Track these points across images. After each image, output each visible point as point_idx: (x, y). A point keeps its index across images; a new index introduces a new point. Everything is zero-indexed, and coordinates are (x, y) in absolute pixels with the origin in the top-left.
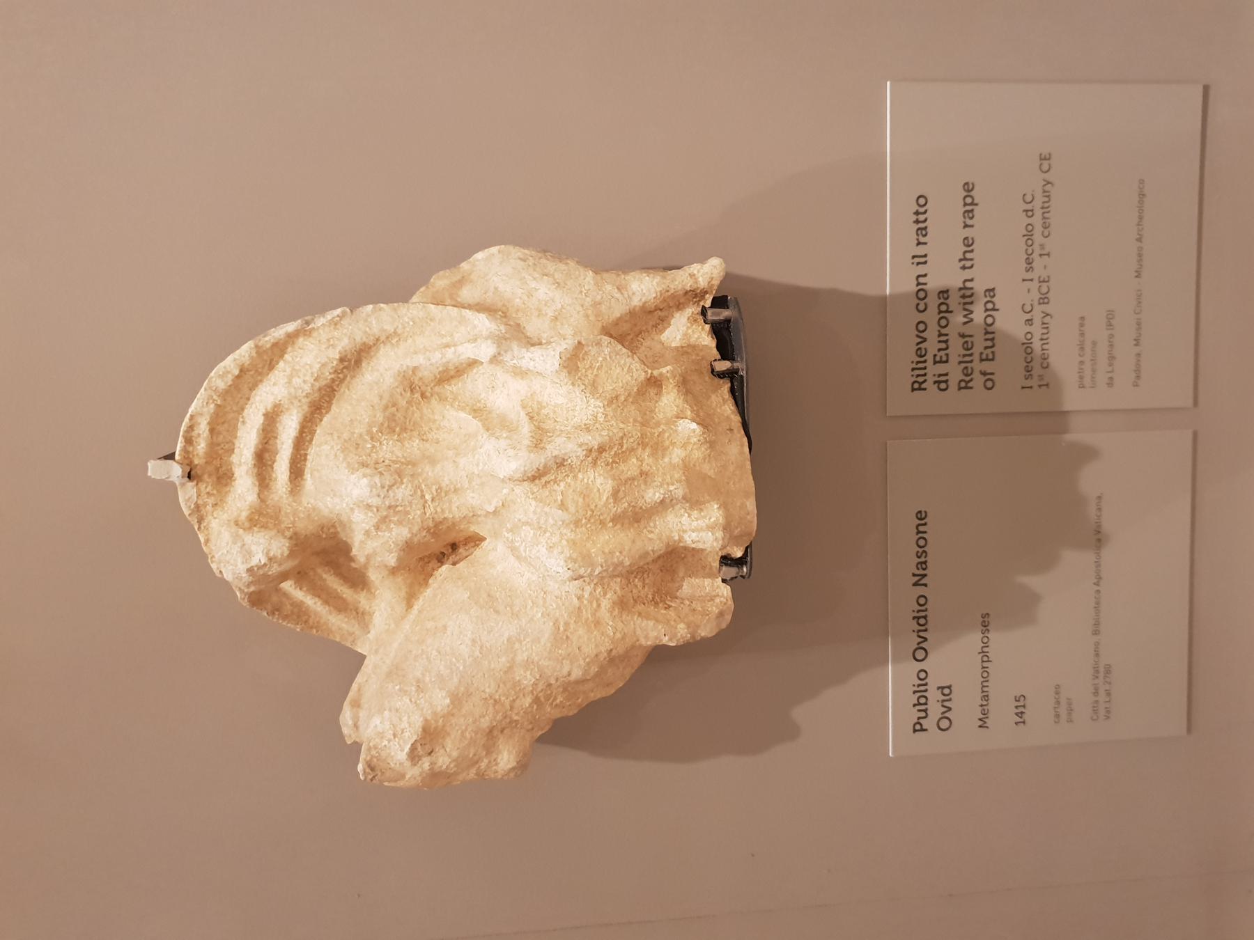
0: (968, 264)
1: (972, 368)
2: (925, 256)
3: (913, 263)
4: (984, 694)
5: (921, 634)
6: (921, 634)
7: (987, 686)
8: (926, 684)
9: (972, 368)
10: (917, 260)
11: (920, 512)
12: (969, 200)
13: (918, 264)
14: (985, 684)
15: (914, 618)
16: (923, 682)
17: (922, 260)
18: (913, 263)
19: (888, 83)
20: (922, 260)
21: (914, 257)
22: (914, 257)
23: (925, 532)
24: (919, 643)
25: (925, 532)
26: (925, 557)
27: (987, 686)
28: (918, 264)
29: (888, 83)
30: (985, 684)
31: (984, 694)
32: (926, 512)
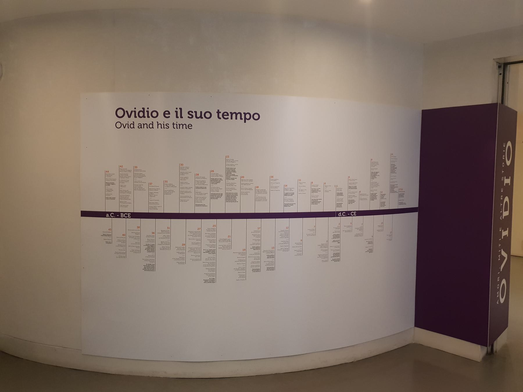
0: (175, 126)
1: (228, 118)
2: (181, 117)
3: (177, 109)
4: (142, 125)
5: (133, 113)
6: (133, 113)
7: (236, 119)
8: (148, 117)
9: (228, 118)
10: (179, 111)
11: (169, 113)
12: (248, 116)
13: (176, 112)
14: (184, 126)
15: (144, 109)
16: (150, 115)
17: (179, 115)
18: (177, 109)
19: (508, 228)
20: (179, 115)
21: (181, 109)
22: (181, 109)
23: (201, 112)
24: (127, 112)
25: (201, 112)
26: (192, 112)
27: (236, 119)
28: (176, 112)
29: (508, 228)
30: (184, 126)
31: (142, 125)
32: (169, 117)
